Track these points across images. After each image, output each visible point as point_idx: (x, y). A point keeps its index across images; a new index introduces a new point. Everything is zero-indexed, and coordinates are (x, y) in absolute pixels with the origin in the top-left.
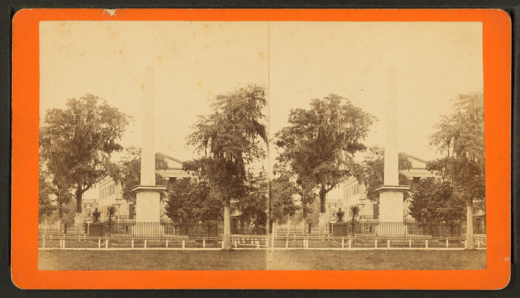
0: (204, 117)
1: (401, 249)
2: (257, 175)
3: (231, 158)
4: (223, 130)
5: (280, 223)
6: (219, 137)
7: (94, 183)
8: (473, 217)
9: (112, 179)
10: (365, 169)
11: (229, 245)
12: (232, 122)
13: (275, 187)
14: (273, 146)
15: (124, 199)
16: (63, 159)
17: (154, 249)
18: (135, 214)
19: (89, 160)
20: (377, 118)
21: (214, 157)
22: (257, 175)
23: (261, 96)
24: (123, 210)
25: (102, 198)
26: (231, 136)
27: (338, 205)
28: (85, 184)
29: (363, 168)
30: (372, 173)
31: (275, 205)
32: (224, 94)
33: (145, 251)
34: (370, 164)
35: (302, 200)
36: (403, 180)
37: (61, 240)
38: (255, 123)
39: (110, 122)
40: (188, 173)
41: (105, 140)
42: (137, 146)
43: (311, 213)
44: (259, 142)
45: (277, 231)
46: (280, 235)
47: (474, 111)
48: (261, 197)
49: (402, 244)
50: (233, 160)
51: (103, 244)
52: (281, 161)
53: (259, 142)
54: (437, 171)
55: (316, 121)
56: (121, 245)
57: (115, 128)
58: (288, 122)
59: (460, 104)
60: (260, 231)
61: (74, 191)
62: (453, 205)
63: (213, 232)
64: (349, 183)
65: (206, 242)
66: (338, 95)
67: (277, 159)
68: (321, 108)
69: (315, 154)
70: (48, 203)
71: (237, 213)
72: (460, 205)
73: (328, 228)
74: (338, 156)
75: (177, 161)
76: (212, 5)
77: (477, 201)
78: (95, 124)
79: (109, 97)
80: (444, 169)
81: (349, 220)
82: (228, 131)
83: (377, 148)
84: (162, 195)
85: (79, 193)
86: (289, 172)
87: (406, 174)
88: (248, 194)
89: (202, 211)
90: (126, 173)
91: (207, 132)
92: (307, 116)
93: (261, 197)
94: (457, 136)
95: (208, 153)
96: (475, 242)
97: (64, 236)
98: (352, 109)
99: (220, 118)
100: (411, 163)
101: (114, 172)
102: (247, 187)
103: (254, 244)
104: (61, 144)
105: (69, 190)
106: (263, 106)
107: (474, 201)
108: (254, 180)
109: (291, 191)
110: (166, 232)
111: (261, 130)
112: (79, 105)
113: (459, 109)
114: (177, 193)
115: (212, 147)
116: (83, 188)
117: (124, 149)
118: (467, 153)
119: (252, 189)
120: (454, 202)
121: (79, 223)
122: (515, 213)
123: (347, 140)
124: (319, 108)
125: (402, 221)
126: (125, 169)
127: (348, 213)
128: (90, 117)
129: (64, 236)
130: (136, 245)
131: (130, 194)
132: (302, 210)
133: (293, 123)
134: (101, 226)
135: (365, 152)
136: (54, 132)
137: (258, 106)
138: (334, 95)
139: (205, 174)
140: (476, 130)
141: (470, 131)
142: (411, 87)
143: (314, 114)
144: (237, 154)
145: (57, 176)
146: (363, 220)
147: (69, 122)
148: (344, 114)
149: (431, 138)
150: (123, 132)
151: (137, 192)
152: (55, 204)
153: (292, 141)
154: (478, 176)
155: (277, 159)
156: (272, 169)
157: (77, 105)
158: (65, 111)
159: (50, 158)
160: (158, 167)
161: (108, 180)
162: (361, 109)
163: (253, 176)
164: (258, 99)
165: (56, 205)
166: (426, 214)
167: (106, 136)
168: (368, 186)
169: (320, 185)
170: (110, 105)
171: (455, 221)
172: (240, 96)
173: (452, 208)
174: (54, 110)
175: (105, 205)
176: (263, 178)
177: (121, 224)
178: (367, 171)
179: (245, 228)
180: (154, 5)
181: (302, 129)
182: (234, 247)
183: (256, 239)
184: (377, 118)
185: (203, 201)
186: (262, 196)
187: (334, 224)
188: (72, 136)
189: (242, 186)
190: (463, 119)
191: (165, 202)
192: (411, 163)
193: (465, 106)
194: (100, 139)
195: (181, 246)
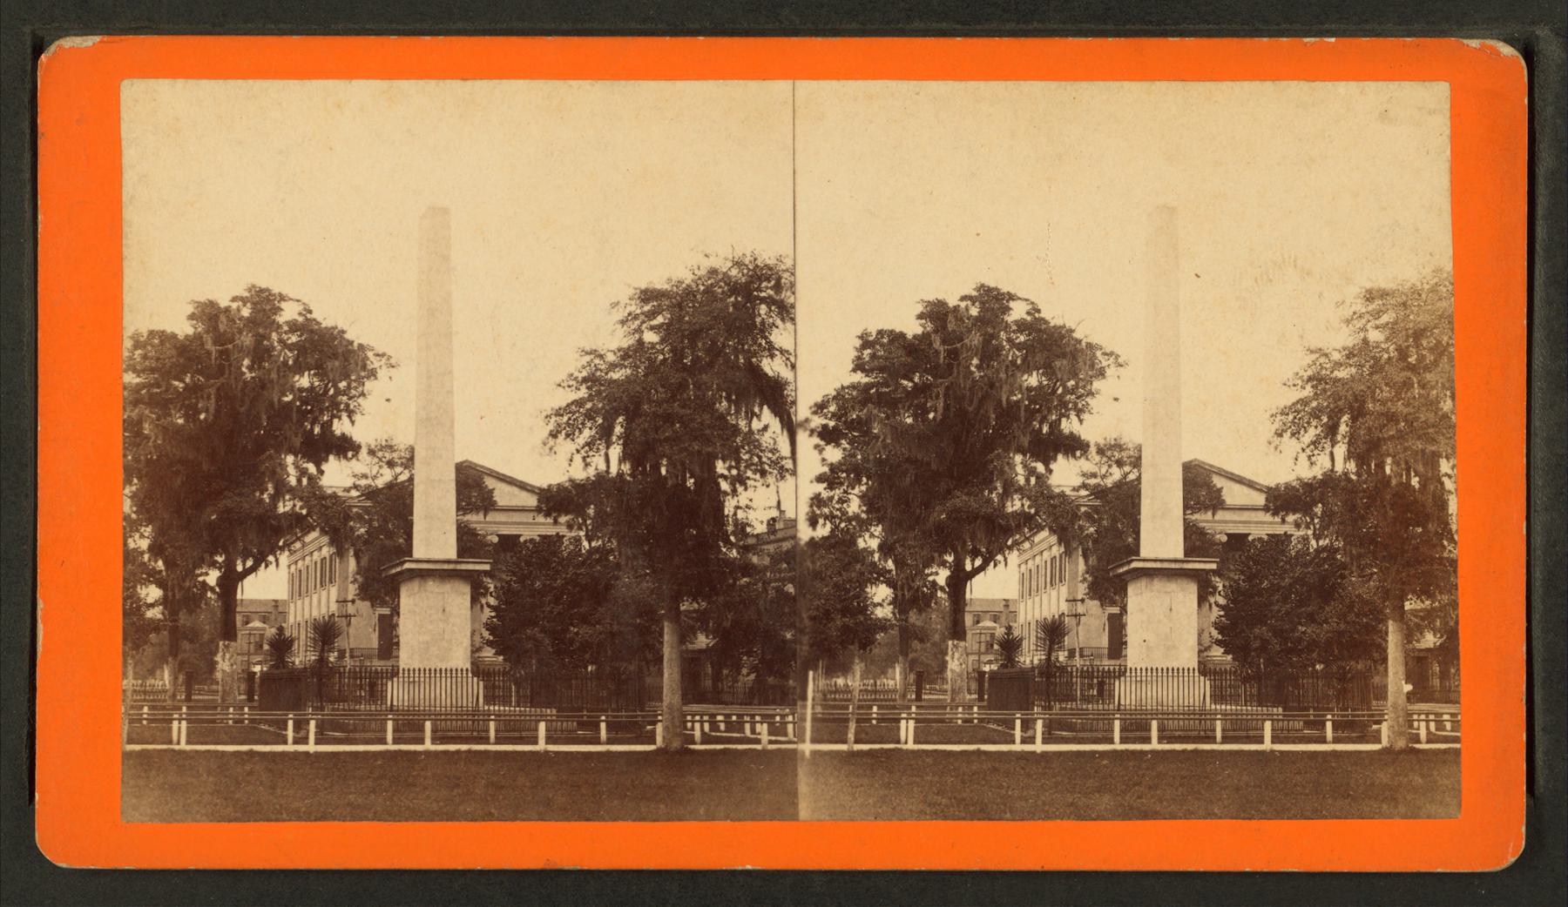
0: (601, 357)
1: (464, 747)
2: (761, 528)
3: (1408, 475)
4: (659, 394)
5: (830, 672)
7: (1001, 551)
8: (682, 652)
9: (325, 539)
10: (1083, 509)
12: (685, 368)
13: (813, 562)
14: (805, 442)
15: (363, 599)
16: (179, 481)
17: (452, 747)
18: (398, 644)
19: (988, 483)
20: (1117, 356)
21: (1358, 474)
22: (761, 528)
23: (771, 292)
24: (1090, 631)
27: (1003, 619)
28: (975, 553)
29: (351, 507)
30: (1105, 523)
31: (812, 618)
32: (660, 284)
33: (1152, 752)
34: (1099, 492)
35: (894, 602)
36: (1196, 541)
37: (175, 723)
38: (756, 372)
39: (1049, 370)
40: (1283, 521)
41: (1036, 424)
42: (403, 439)
43: (922, 641)
44: (766, 428)
46: (834, 707)
47: (683, 336)
50: (1415, 481)
51: (1030, 733)
52: (831, 487)
53: (766, 428)
54: (1298, 515)
55: (937, 366)
56: (1081, 735)
57: (335, 386)
59: (1367, 316)
60: (776, 689)
61: (942, 576)
62: (1345, 616)
63: (630, 701)
64: (1036, 550)
66: (276, 290)
67: (820, 479)
68: (950, 327)
69: (934, 467)
70: (863, 610)
71: (702, 641)
72: (1366, 615)
73: (974, 686)
74: (1002, 472)
75: (1251, 485)
76: (633, 25)
77: (1419, 605)
78: (274, 376)
79: (322, 294)
80: (1318, 509)
81: (1036, 662)
82: (674, 396)
83: (391, 448)
84: (477, 594)
85: (959, 580)
86: (856, 517)
87: (478, 526)
89: (1322, 632)
90: (370, 522)
91: (1337, 397)
92: (909, 354)
93: (772, 593)
94: (1358, 413)
95: (612, 461)
96: (1411, 727)
97: (914, 709)
98: (1044, 331)
99: (649, 359)
100: (1220, 490)
101: (1058, 515)
102: (729, 562)
103: (753, 731)
104: (900, 433)
105: (198, 572)
106: (779, 322)
107: (1407, 606)
108: (751, 541)
109: (862, 574)
110: (490, 698)
111: (775, 395)
113: (1364, 329)
114: (1250, 579)
115: (1350, 444)
116: (968, 567)
117: (364, 451)
118: (1389, 460)
119: (747, 569)
120: (1351, 607)
121: (958, 669)
122: (1536, 644)
124: (944, 327)
125: (1194, 664)
127: (1033, 639)
128: (261, 353)
129: (914, 709)
130: (1340, 734)
131: (1109, 585)
132: (895, 632)
133: (867, 372)
134: (296, 677)
135: (1083, 460)
136: (882, 401)
137: (763, 322)
139: (605, 524)
140: (1417, 391)
141: (674, 396)
142: (1223, 260)
144: (1425, 464)
146: (1078, 662)
147: (926, 371)
148: (1020, 347)
149: (1279, 417)
150: (360, 400)
151: (1127, 577)
152: (155, 613)
153: (862, 425)
155: (820, 479)
156: (804, 509)
157: (223, 318)
158: (915, 337)
159: (140, 479)
160: (464, 505)
161: (317, 546)
162: (1072, 331)
163: (748, 530)
164: (763, 300)
165: (160, 616)
166: (1264, 647)
167: (1038, 411)
168: (1093, 560)
169: (950, 558)
170: (319, 319)
172: (709, 291)
173: (1342, 626)
175: (1037, 616)
176: (779, 535)
177: (354, 674)
178: (1088, 516)
179: (726, 685)
180: (460, 25)
182: (1419, 742)
183: (758, 718)
184: (1117, 356)
185: (1327, 602)
186: (778, 590)
187: (992, 672)
188: (207, 411)
189: (1441, 558)
190: (1377, 360)
191: (487, 610)
192: (1220, 490)
193: (654, 322)
195: (1260, 740)
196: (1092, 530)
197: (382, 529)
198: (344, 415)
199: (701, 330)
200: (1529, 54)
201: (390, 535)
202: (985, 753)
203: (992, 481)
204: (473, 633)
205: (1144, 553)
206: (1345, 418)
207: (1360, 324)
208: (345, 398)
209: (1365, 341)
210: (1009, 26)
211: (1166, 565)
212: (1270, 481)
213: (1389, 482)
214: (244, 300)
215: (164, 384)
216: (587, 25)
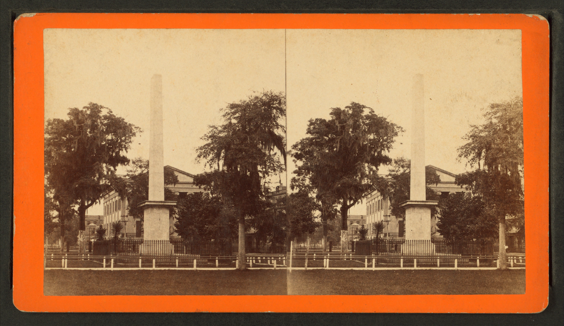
0: (216, 128)
1: (167, 269)
2: (274, 190)
3: (507, 171)
4: (237, 142)
5: (299, 241)
6: (233, 149)
7: (360, 198)
9: (117, 194)
10: (390, 183)
11: (244, 264)
12: (246, 132)
13: (293, 202)
14: (290, 159)
15: (130, 215)
17: (163, 269)
18: (143, 231)
19: (355, 174)
20: (402, 128)
21: (489, 170)
22: (274, 190)
23: (277, 105)
24: (392, 227)
25: (107, 214)
26: (246, 148)
27: (361, 222)
28: (351, 199)
29: (126, 182)
32: (238, 102)
33: (414, 270)
34: (395, 177)
35: (321, 216)
36: (430, 194)
37: (63, 260)
38: (272, 134)
39: (377, 133)
40: (462, 187)
41: (373, 153)
42: (145, 158)
43: (331, 230)
44: (275, 154)
45: (295, 250)
48: (278, 213)
49: (430, 264)
51: (370, 264)
52: (299, 175)
53: (275, 154)
54: (467, 185)
55: (337, 132)
57: (383, 139)
58: (307, 133)
59: (492, 114)
60: (279, 248)
61: (339, 207)
62: (484, 221)
63: (227, 252)
64: (373, 198)
65: (480, 261)
66: (361, 104)
67: (295, 172)
68: (342, 118)
69: (336, 168)
70: (310, 219)
71: (253, 230)
72: (491, 221)
73: (350, 246)
74: (360, 170)
75: (450, 174)
76: (228, 9)
77: (510, 218)
79: (116, 106)
80: (474, 183)
81: (373, 238)
83: (141, 161)
84: (172, 213)
85: (345, 208)
86: (308, 186)
87: (172, 189)
88: (264, 210)
92: (327, 127)
93: (278, 213)
94: (488, 149)
95: (220, 166)
96: (508, 261)
97: (329, 255)
99: (233, 129)
100: (439, 176)
102: (262, 202)
103: (271, 263)
104: (324, 156)
105: (71, 205)
106: (280, 116)
107: (506, 218)
108: (270, 194)
109: (310, 206)
110: (176, 251)
111: (279, 142)
112: (344, 115)
113: (491, 118)
114: (188, 208)
115: (485, 159)
116: (348, 204)
117: (131, 162)
118: (500, 165)
119: (269, 204)
120: (486, 218)
121: (344, 241)
122: (552, 231)
123: (370, 151)
124: (340, 118)
125: (429, 239)
126: (131, 183)
127: (372, 230)
128: (94, 127)
129: (329, 255)
130: (482, 264)
131: (399, 210)
132: (322, 227)
133: (312, 134)
134: (106, 243)
135: (389, 165)
136: (317, 144)
137: (274, 116)
138: (356, 104)
139: (218, 188)
142: (440, 94)
143: (335, 124)
145: (58, 191)
146: (388, 238)
147: (333, 133)
148: (367, 125)
149: (460, 150)
150: (130, 144)
151: (406, 208)
152: (56, 220)
153: (310, 153)
154: (511, 190)
155: (295, 172)
156: (289, 183)
158: (329, 121)
159: (50, 172)
160: (167, 182)
161: (114, 196)
162: (386, 119)
163: (269, 190)
164: (274, 108)
165: (58, 222)
166: (455, 233)
167: (374, 148)
168: (393, 201)
169: (342, 201)
170: (115, 115)
171: (225, 239)
172: (255, 104)
173: (483, 225)
174: (54, 120)
175: (373, 222)
176: (280, 192)
177: (127, 242)
178: (391, 185)
180: (165, 9)
181: (322, 140)
182: (510, 267)
183: (273, 258)
184: (402, 128)
185: (477, 217)
186: (280, 212)
188: (74, 148)
189: (518, 201)
190: (495, 129)
192: (439, 176)
193: (235, 116)
194: (366, 151)
195: (453, 266)
196: (393, 190)
197: (137, 190)
198: (124, 149)
199: (252, 119)
200: (550, 19)
201: (140, 192)
202: (354, 270)
203: (357, 173)
204: (170, 228)
205: (411, 199)
206: (484, 150)
207: (489, 116)
208: (124, 143)
209: (491, 123)
210: (363, 9)
211: (419, 203)
212: (457, 173)
213: (500, 173)
214: (88, 108)
215: (59, 138)
216: (211, 9)
